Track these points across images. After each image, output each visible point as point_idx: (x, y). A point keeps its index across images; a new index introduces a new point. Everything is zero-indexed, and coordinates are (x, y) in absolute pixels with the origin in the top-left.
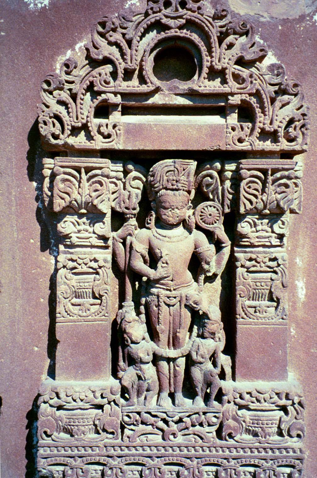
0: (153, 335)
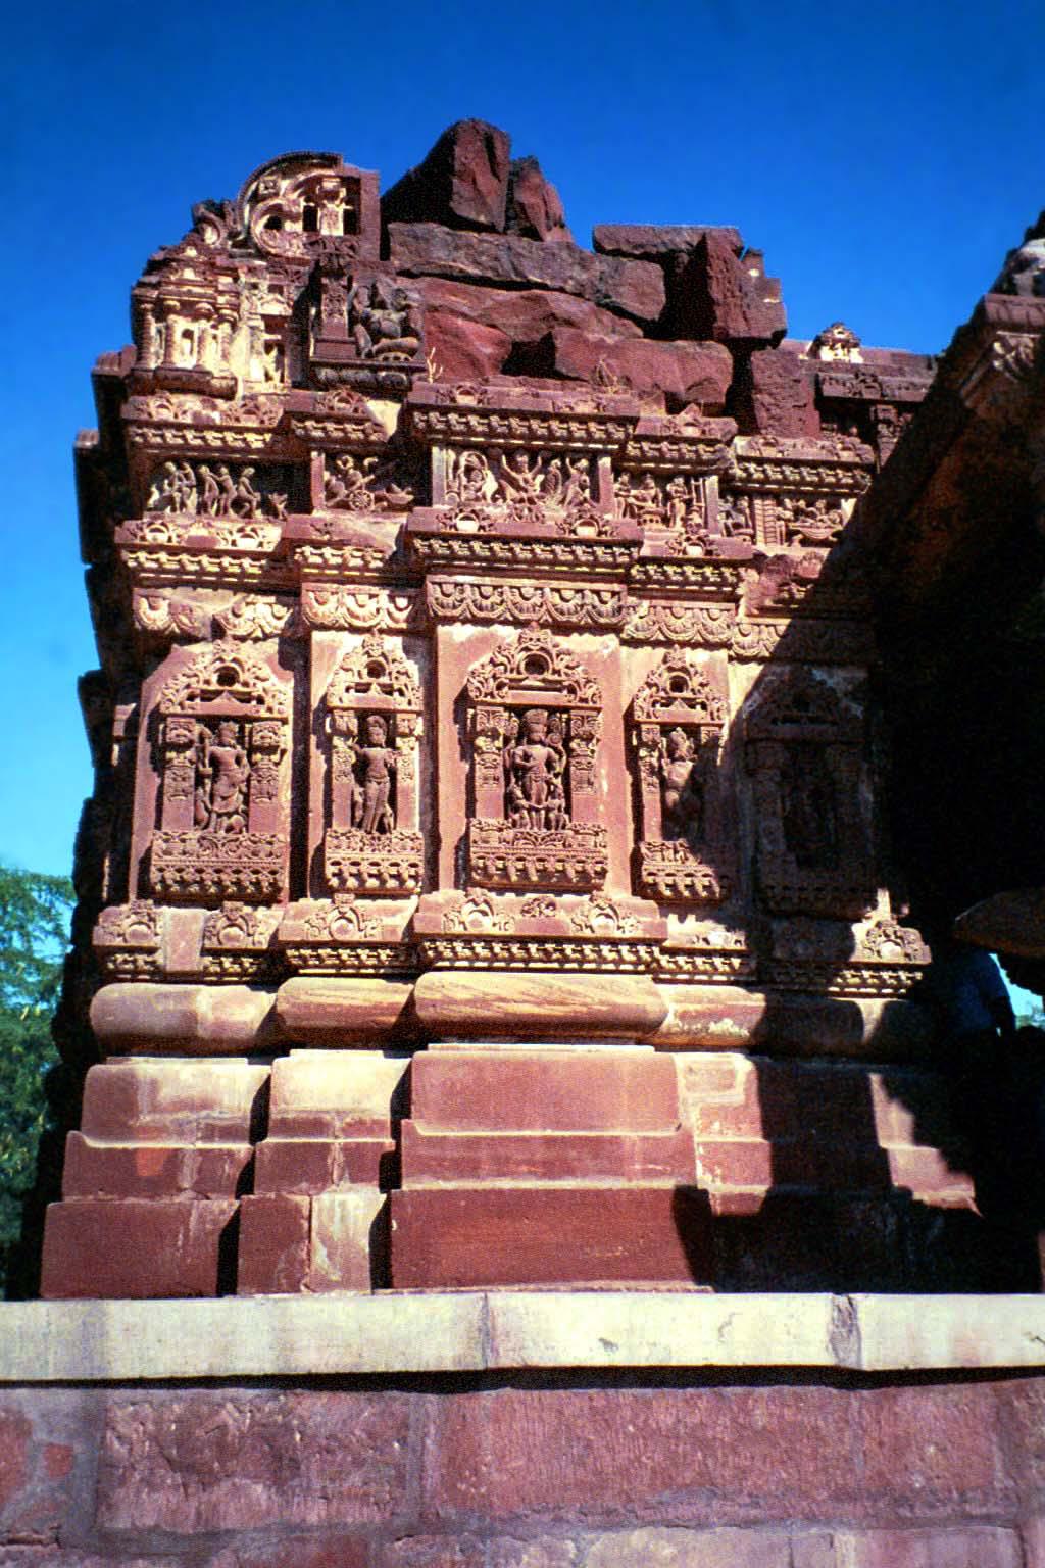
0: (527, 797)
